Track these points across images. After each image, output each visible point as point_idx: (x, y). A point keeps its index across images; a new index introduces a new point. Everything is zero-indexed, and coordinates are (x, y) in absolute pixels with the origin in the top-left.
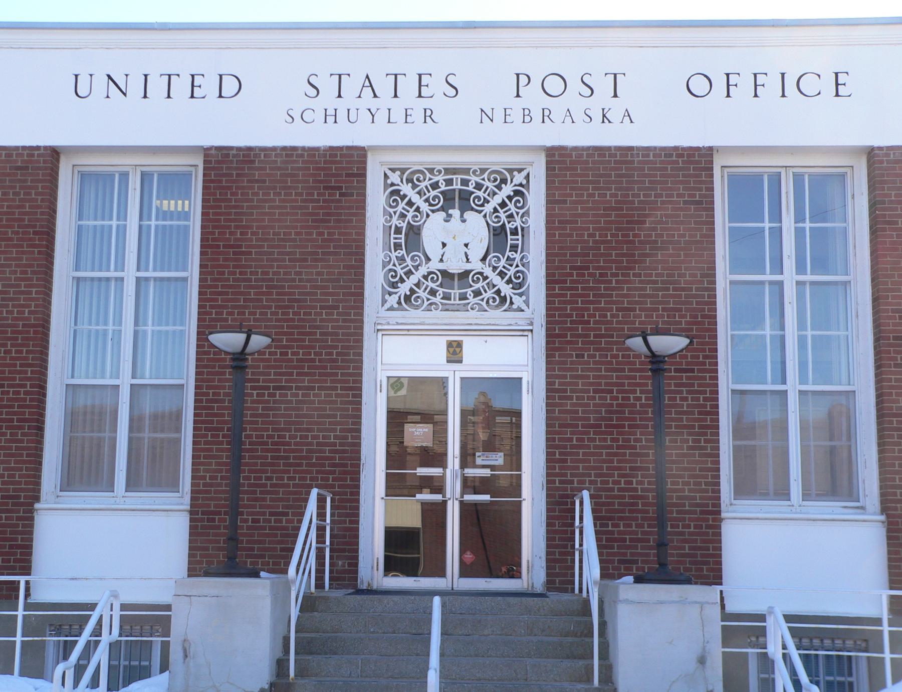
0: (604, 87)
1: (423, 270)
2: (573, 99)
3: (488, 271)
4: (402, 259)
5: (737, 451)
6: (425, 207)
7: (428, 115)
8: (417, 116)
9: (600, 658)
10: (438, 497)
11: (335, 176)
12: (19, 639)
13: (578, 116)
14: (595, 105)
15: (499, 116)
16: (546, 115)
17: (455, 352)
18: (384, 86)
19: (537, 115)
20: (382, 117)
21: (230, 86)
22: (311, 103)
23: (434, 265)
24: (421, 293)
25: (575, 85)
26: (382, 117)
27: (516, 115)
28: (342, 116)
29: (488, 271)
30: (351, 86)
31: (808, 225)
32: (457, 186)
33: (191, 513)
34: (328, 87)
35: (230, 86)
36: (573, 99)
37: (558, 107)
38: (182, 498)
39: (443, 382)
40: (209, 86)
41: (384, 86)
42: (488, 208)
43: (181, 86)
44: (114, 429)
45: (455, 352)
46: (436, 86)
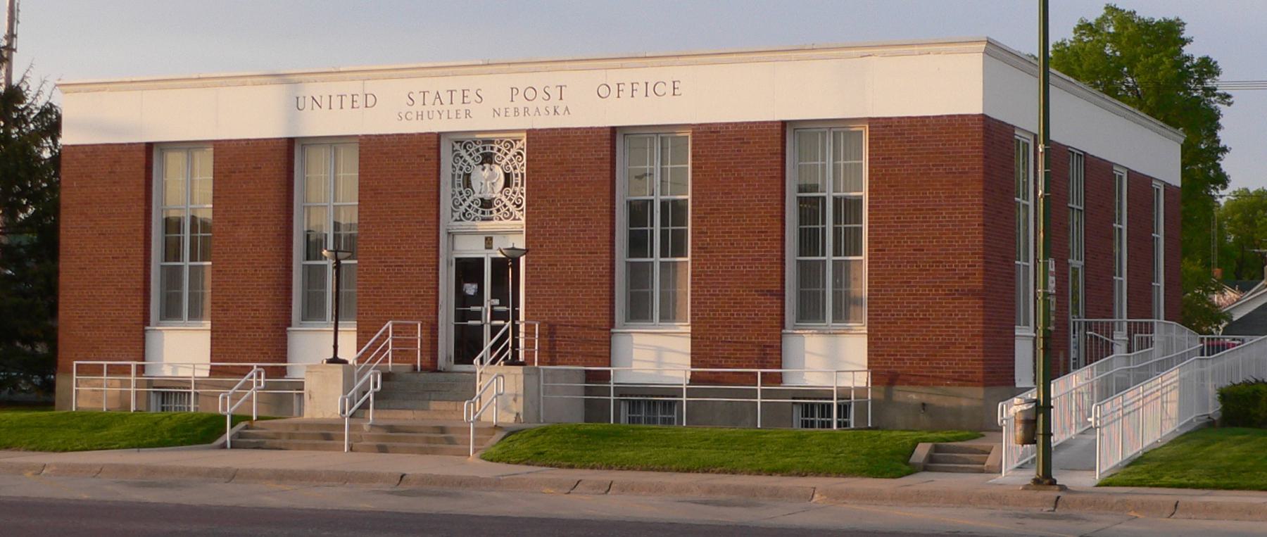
0: (555, 93)
1: (471, 198)
2: (540, 103)
3: (503, 198)
4: (498, 210)
5: (835, 293)
6: (472, 162)
7: (468, 113)
8: (462, 114)
9: (835, 285)
10: (478, 322)
11: (427, 148)
12: (612, 398)
13: (542, 111)
14: (550, 105)
15: (503, 113)
16: (526, 110)
17: (489, 243)
18: (445, 97)
19: (521, 111)
20: (444, 115)
21: (371, 100)
22: (411, 109)
23: (477, 195)
24: (470, 211)
25: (541, 94)
26: (444, 115)
27: (511, 112)
28: (425, 114)
29: (503, 198)
30: (430, 98)
31: (820, 226)
32: (488, 150)
33: (212, 331)
34: (418, 98)
35: (370, 101)
36: (540, 103)
38: (207, 324)
39: (481, 260)
40: (360, 101)
41: (445, 97)
42: (503, 163)
44: (824, 286)
45: (489, 243)
46: (471, 96)
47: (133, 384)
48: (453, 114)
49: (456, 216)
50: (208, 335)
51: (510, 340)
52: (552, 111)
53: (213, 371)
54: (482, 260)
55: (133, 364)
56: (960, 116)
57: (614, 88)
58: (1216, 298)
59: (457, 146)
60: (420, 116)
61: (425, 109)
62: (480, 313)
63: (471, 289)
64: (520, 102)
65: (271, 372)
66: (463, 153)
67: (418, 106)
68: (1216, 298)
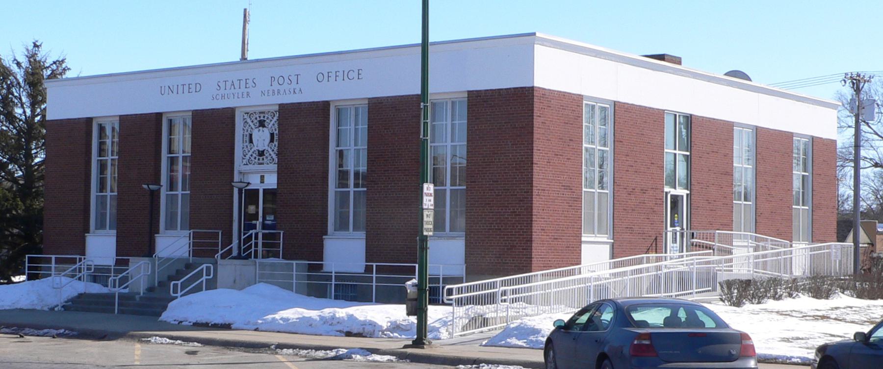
0: (294, 79)
2: (286, 86)
5: (264, 208)
8: (245, 94)
14: (240, 91)
22: (218, 92)
23: (255, 148)
24: (252, 158)
25: (287, 80)
27: (271, 93)
37: (282, 88)
41: (237, 84)
43: (229, 84)
47: (53, 269)
48: (240, 96)
49: (245, 161)
50: (115, 238)
51: (243, 238)
52: (292, 91)
53: (118, 262)
54: (258, 190)
55: (78, 257)
56: (521, 88)
57: (326, 75)
58: (683, 320)
59: (246, 116)
60: (223, 97)
61: (226, 92)
62: (255, 225)
63: (252, 209)
64: (276, 86)
65: (311, 268)
66: (249, 120)
67: (222, 91)
68: (683, 320)
